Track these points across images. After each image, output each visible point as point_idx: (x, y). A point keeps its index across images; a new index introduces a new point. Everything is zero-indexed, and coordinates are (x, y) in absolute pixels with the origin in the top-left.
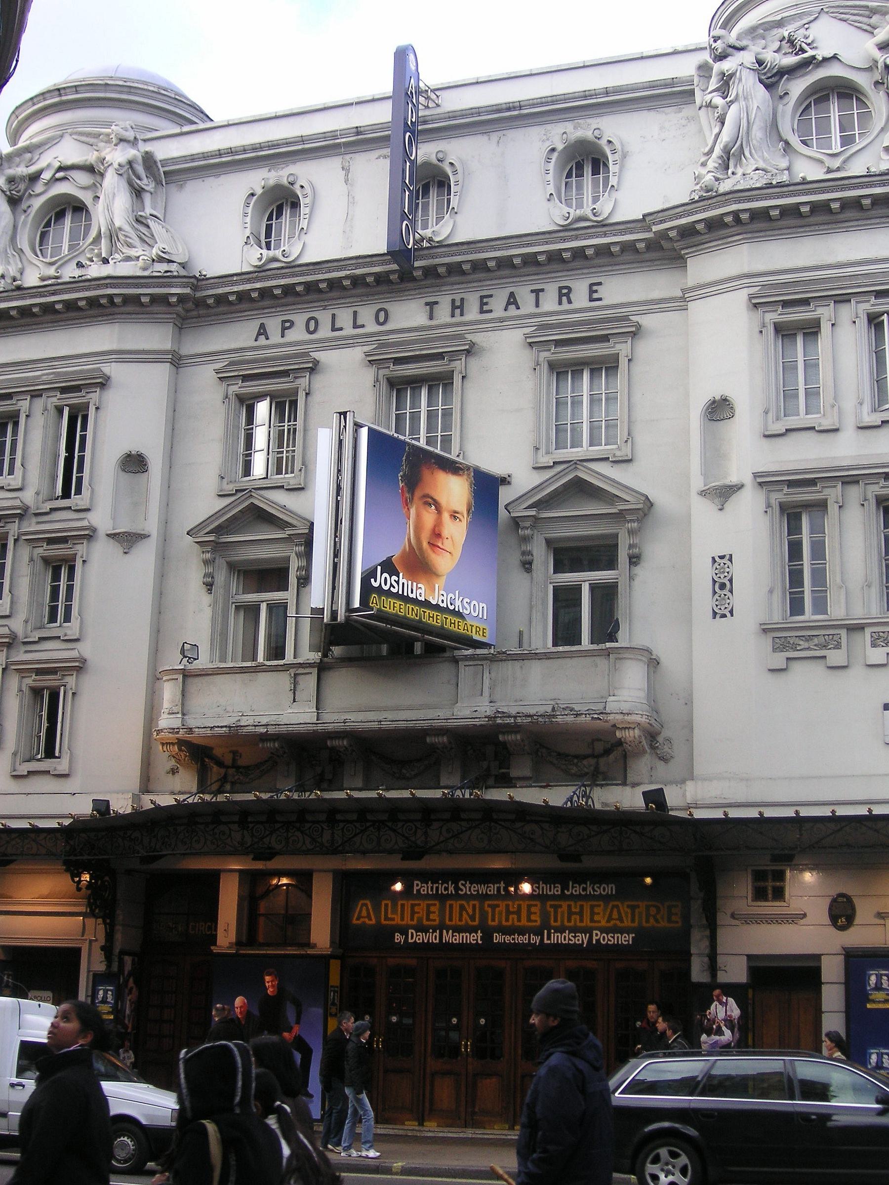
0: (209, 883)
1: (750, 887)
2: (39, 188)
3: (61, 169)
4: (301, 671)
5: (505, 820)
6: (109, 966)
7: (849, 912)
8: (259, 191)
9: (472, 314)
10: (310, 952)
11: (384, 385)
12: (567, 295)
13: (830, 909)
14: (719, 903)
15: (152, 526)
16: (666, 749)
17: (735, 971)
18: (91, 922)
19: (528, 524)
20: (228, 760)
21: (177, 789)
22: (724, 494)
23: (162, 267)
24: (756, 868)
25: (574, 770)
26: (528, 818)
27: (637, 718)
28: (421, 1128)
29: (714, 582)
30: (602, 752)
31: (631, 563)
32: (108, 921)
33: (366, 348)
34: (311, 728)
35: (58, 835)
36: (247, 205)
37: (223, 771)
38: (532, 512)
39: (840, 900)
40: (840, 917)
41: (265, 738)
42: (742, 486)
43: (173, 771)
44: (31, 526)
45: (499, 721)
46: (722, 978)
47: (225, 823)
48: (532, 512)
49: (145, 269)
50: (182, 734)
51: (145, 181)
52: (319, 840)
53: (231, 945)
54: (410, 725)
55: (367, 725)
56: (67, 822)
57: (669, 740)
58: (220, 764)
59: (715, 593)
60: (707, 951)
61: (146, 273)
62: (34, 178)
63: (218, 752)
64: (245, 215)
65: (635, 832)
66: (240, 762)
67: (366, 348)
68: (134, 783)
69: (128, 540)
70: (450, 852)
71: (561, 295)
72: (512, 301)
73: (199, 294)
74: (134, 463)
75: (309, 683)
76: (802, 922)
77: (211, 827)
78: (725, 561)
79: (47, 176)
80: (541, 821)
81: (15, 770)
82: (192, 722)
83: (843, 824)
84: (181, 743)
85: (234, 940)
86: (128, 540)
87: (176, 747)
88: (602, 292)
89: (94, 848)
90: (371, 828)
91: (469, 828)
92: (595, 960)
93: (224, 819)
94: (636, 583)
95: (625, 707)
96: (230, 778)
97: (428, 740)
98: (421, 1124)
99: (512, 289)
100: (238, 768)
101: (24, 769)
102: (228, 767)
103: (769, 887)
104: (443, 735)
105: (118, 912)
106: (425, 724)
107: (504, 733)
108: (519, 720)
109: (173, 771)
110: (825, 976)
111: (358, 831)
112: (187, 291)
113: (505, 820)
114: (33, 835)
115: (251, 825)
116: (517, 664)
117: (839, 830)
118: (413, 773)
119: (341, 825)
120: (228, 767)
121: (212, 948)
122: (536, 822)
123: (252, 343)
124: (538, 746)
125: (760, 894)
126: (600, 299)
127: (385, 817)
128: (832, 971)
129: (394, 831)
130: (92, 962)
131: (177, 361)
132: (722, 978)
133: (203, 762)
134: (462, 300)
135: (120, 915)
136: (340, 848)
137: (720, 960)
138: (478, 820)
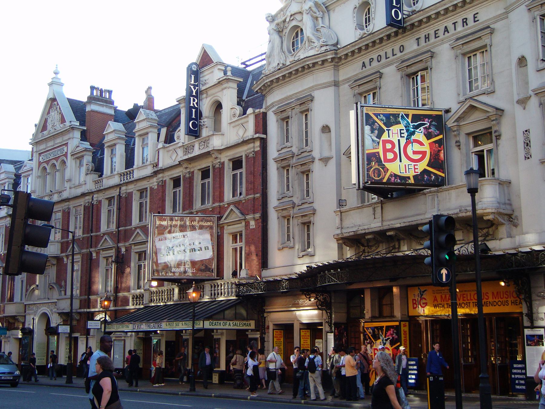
2: (286, 25)
3: (291, 15)
4: (376, 206)
8: (358, 6)
9: (432, 39)
11: (405, 77)
12: (466, 22)
14: (532, 290)
15: (333, 153)
16: (516, 221)
19: (455, 129)
22: (523, 102)
23: (324, 48)
27: (490, 211)
29: (524, 143)
31: (497, 139)
33: (395, 65)
36: (354, 13)
37: (363, 248)
38: (455, 124)
42: (531, 96)
44: (294, 160)
48: (455, 124)
49: (318, 51)
51: (318, 13)
57: (516, 217)
59: (525, 148)
61: (319, 53)
62: (284, 21)
64: (354, 17)
67: (395, 65)
69: (325, 160)
70: (404, 278)
71: (463, 22)
72: (446, 30)
73: (339, 56)
74: (326, 129)
75: (379, 210)
78: (527, 132)
79: (288, 20)
82: (344, 231)
84: (342, 239)
86: (325, 160)
88: (479, 17)
94: (500, 148)
95: (484, 206)
96: (366, 251)
99: (445, 25)
101: (301, 254)
105: (333, 307)
112: (334, 56)
116: (447, 192)
123: (361, 71)
126: (478, 20)
131: (336, 84)
134: (463, 26)
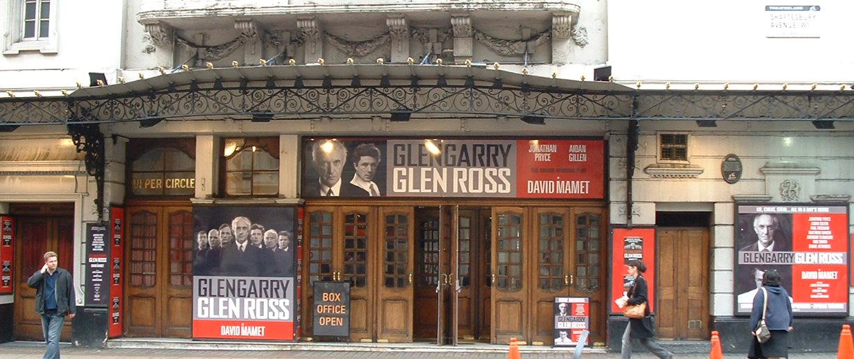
0: (187, 145)
1: (659, 147)
5: (484, 87)
6: (101, 216)
7: (738, 170)
10: (279, 201)
13: (722, 167)
17: (646, 215)
18: (82, 180)
20: (199, 41)
21: (151, 65)
24: (664, 133)
25: (506, 51)
26: (504, 86)
28: (374, 345)
30: (529, 36)
32: (99, 178)
34: (285, 10)
35: (61, 103)
37: (194, 50)
39: (730, 159)
40: (731, 173)
41: (241, 19)
43: (149, 50)
45: (453, 7)
46: (636, 220)
47: (226, 89)
50: (164, 16)
52: (316, 103)
53: (208, 197)
54: (374, 9)
55: (335, 9)
56: (69, 93)
58: (192, 44)
60: (624, 199)
63: (188, 35)
65: (589, 100)
66: (208, 43)
68: (117, 62)
76: (700, 176)
77: (213, 92)
80: (512, 88)
81: (7, 50)
83: (667, 97)
84: (161, 23)
85: (211, 193)
87: (159, 28)
89: (87, 116)
90: (364, 93)
91: (454, 94)
92: (523, 207)
93: (224, 85)
96: (201, 56)
97: (388, 23)
98: (375, 340)
100: (208, 48)
101: (15, 49)
102: (198, 47)
103: (674, 147)
104: (401, 18)
106: (386, 9)
107: (455, 18)
108: (472, 6)
109: (149, 50)
110: (718, 219)
111: (352, 96)
113: (484, 87)
114: (37, 104)
115: (251, 91)
117: (758, 102)
118: (366, 52)
119: (336, 90)
120: (198, 47)
121: (191, 199)
122: (510, 89)
124: (475, 31)
125: (666, 154)
127: (378, 83)
128: (723, 215)
129: (385, 95)
130: (85, 213)
132: (636, 220)
133: (176, 41)
135: (109, 173)
136: (336, 110)
137: (635, 206)
138: (462, 86)
